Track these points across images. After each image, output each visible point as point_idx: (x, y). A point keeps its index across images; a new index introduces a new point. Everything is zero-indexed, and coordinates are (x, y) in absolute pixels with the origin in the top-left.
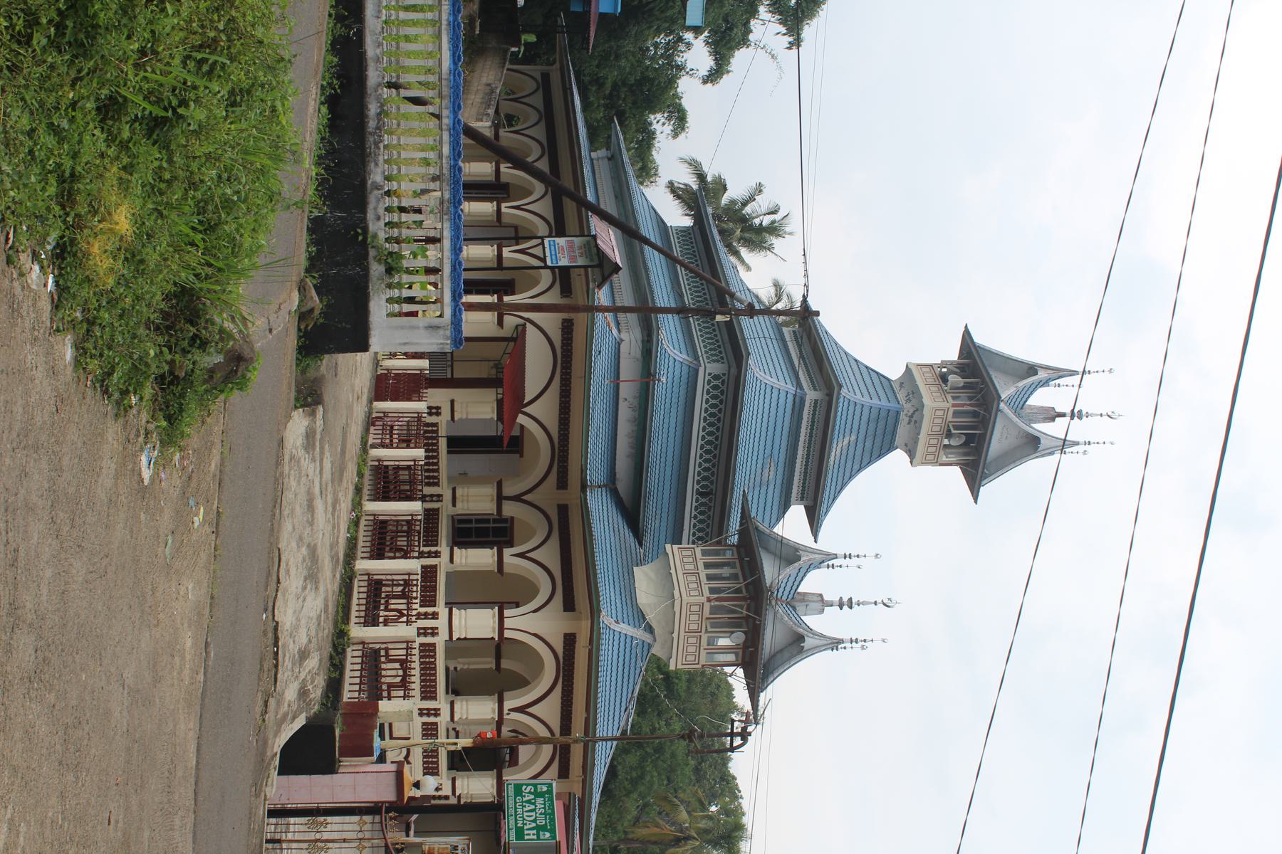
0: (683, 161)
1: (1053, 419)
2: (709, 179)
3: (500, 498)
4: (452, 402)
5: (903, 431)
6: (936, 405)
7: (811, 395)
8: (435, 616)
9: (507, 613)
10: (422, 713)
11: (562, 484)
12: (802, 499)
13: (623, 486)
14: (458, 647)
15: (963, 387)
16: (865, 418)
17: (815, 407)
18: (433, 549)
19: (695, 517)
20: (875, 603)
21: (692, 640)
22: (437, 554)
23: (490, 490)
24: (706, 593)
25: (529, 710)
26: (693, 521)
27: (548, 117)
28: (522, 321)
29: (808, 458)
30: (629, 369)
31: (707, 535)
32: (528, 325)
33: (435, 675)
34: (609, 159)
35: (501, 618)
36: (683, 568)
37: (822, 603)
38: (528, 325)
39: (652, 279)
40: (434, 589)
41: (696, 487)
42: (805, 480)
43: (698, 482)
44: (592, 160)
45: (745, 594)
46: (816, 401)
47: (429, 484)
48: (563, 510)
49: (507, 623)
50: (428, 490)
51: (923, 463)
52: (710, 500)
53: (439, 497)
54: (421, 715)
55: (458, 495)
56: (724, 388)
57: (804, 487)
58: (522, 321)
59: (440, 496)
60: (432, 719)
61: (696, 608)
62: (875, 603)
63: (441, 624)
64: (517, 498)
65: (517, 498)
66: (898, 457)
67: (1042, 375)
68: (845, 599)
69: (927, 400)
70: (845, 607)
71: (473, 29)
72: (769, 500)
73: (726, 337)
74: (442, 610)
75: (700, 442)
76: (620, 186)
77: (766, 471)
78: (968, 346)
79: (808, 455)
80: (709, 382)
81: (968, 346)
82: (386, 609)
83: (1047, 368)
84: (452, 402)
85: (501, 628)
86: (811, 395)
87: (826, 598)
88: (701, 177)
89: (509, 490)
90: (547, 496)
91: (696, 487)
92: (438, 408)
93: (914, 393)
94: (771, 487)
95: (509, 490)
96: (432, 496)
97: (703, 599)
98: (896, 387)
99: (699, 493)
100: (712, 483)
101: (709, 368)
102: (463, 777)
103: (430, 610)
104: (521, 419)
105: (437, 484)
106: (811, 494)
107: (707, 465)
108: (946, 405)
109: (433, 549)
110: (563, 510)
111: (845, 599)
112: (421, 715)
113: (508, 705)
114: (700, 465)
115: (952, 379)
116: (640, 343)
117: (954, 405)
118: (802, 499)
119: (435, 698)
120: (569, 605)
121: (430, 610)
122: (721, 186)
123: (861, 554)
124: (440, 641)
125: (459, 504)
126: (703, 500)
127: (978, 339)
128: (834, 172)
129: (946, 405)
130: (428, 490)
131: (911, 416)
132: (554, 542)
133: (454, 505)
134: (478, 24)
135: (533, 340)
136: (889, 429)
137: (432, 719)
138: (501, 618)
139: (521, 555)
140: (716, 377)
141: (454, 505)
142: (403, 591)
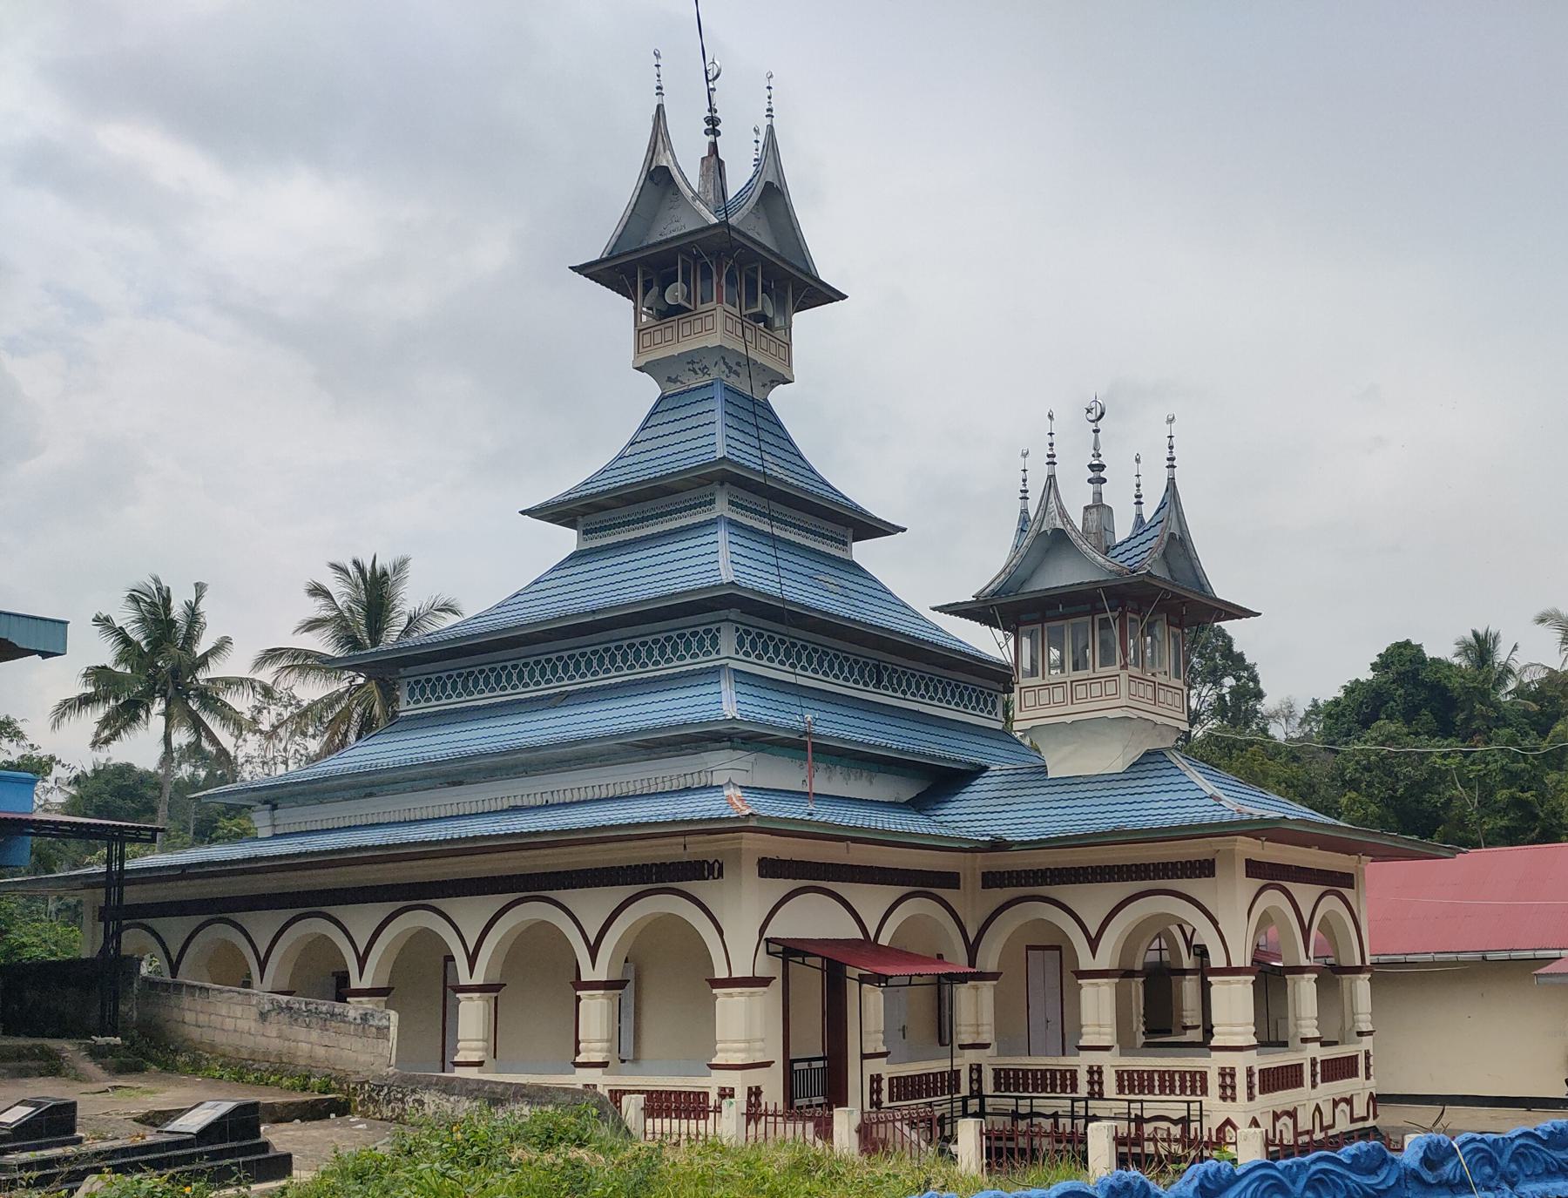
0: (56, 724)
1: (721, 163)
2: (90, 690)
6: (719, 328)
7: (721, 508)
9: (721, 973)
11: (951, 880)
12: (845, 544)
13: (906, 792)
14: (898, 1031)
19: (904, 692)
22: (977, 1069)
26: (908, 696)
27: (219, 909)
29: (800, 528)
30: (787, 775)
34: (275, 807)
35: (731, 982)
36: (1063, 703)
37: (1098, 506)
39: (601, 731)
42: (823, 536)
43: (866, 684)
44: (275, 836)
46: (731, 503)
48: (991, 880)
51: (790, 365)
52: (886, 669)
53: (977, 1069)
56: (754, 631)
57: (832, 539)
59: (1091, 1072)
60: (885, 1085)
62: (1096, 431)
63: (1240, 1062)
64: (972, 950)
65: (972, 950)
66: (778, 398)
68: (1092, 475)
69: (713, 341)
70: (1102, 474)
71: (113, 1048)
72: (861, 589)
73: (659, 626)
76: (579, 759)
77: (831, 587)
78: (612, 271)
81: (612, 271)
86: (721, 508)
87: (1090, 503)
88: (85, 701)
90: (973, 903)
91: (871, 688)
93: (693, 361)
94: (847, 584)
96: (1091, 1083)
97: (1124, 674)
98: (673, 388)
100: (866, 664)
101: (752, 642)
104: (884, 940)
106: (840, 529)
108: (719, 313)
110: (991, 880)
111: (1092, 475)
116: (740, 753)
117: (720, 301)
118: (845, 544)
120: (1205, 868)
122: (98, 674)
123: (1048, 439)
127: (595, 251)
128: (331, 439)
129: (719, 313)
130: (1083, 1089)
131: (730, 368)
133: (986, 1046)
134: (100, 1040)
135: (787, 926)
137: (885, 1085)
138: (731, 982)
139: (362, 961)
140: (741, 643)
141: (986, 1046)
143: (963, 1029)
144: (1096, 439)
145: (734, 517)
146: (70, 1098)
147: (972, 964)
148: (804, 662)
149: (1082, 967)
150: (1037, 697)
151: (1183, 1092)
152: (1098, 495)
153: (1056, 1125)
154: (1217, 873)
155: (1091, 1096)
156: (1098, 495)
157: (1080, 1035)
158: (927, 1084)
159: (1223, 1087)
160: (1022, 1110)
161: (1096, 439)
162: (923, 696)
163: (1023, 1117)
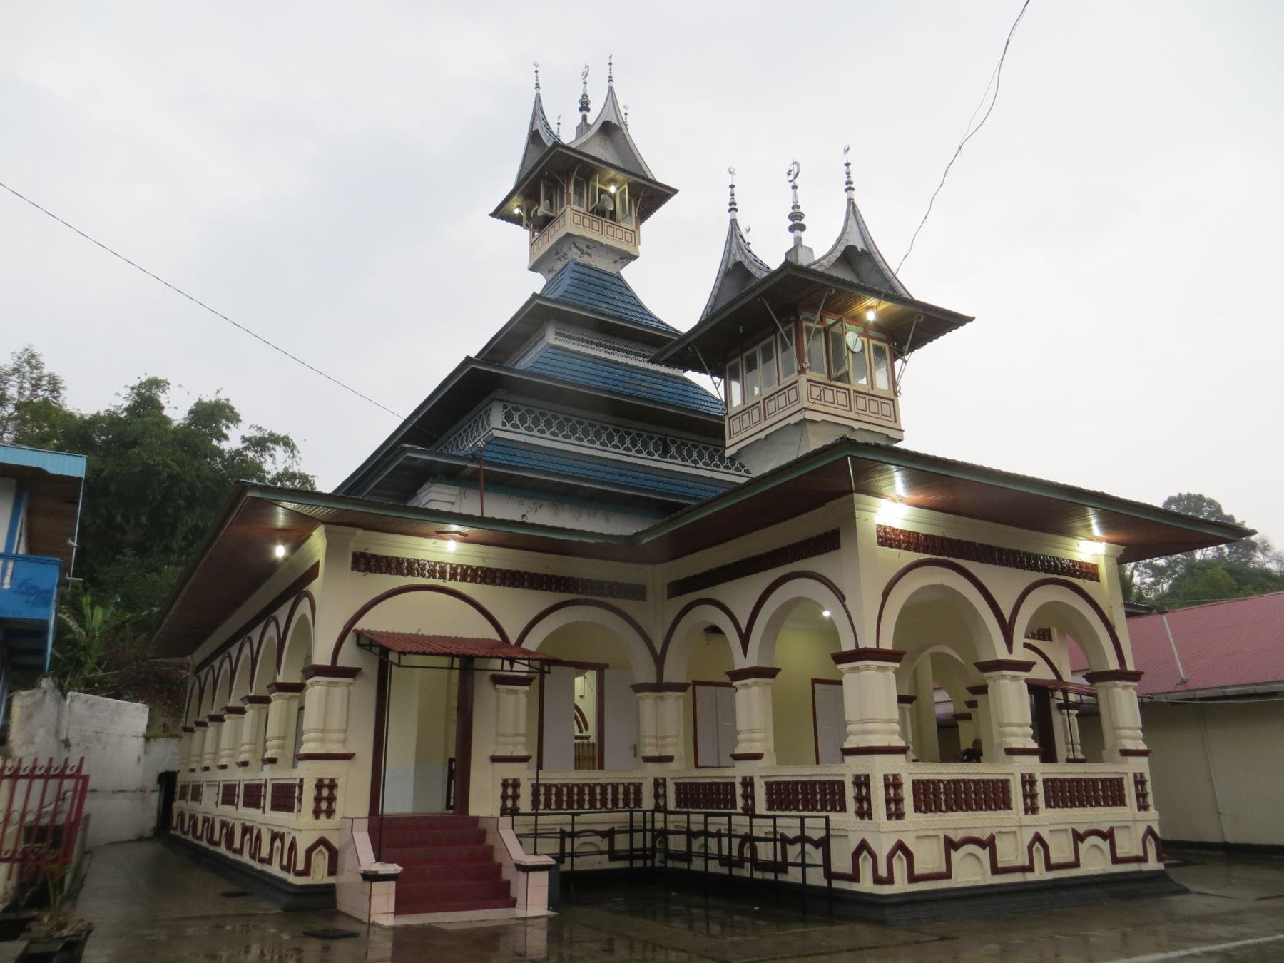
3: (660, 687)
4: (495, 759)
5: (601, 263)
8: (862, 782)
10: (896, 813)
15: (551, 200)
16: (583, 293)
17: (564, 336)
18: (739, 790)
19: (695, 462)
20: (795, 187)
21: (862, 403)
22: (748, 783)
23: (647, 702)
24: (794, 377)
25: (1007, 616)
26: (700, 465)
28: (350, 638)
31: (717, 451)
32: (359, 626)
33: (966, 782)
38: (359, 626)
40: (808, 785)
41: (656, 457)
43: (650, 453)
45: (792, 325)
46: (557, 334)
47: (638, 801)
49: (868, 642)
50: (648, 802)
52: (674, 442)
53: (659, 784)
54: (899, 815)
55: (655, 754)
58: (350, 638)
59: (320, 785)
60: (1040, 788)
61: (816, 391)
63: (878, 768)
64: (659, 661)
65: (659, 661)
66: (630, 274)
67: (538, 126)
74: (850, 768)
75: (597, 445)
79: (623, 351)
80: (515, 426)
82: (855, 877)
83: (533, 123)
84: (495, 759)
85: (876, 654)
89: (646, 674)
91: (656, 457)
92: (505, 784)
95: (646, 674)
96: (657, 796)
99: (665, 452)
100: (651, 438)
102: (1117, 738)
103: (850, 792)
105: (638, 787)
107: (628, 442)
109: (739, 790)
112: (899, 815)
113: (1002, 654)
114: (627, 449)
115: (542, 209)
119: (1005, 784)
121: (850, 792)
124: (908, 771)
125: (668, 752)
126: (673, 450)
130: (648, 802)
131: (582, 251)
132: (722, 592)
136: (596, 274)
137: (1040, 788)
140: (509, 417)
142: (816, 844)
143: (647, 741)
144: (795, 195)
145: (560, 344)
146: (1013, 805)
147: (660, 673)
148: (554, 429)
149: (737, 667)
150: (741, 422)
151: (570, 807)
152: (798, 241)
153: (612, 844)
154: (842, 543)
155: (658, 808)
156: (798, 241)
157: (736, 743)
158: (1096, 790)
159: (318, 799)
160: (694, 828)
161: (795, 195)
162: (717, 466)
163: (697, 835)
